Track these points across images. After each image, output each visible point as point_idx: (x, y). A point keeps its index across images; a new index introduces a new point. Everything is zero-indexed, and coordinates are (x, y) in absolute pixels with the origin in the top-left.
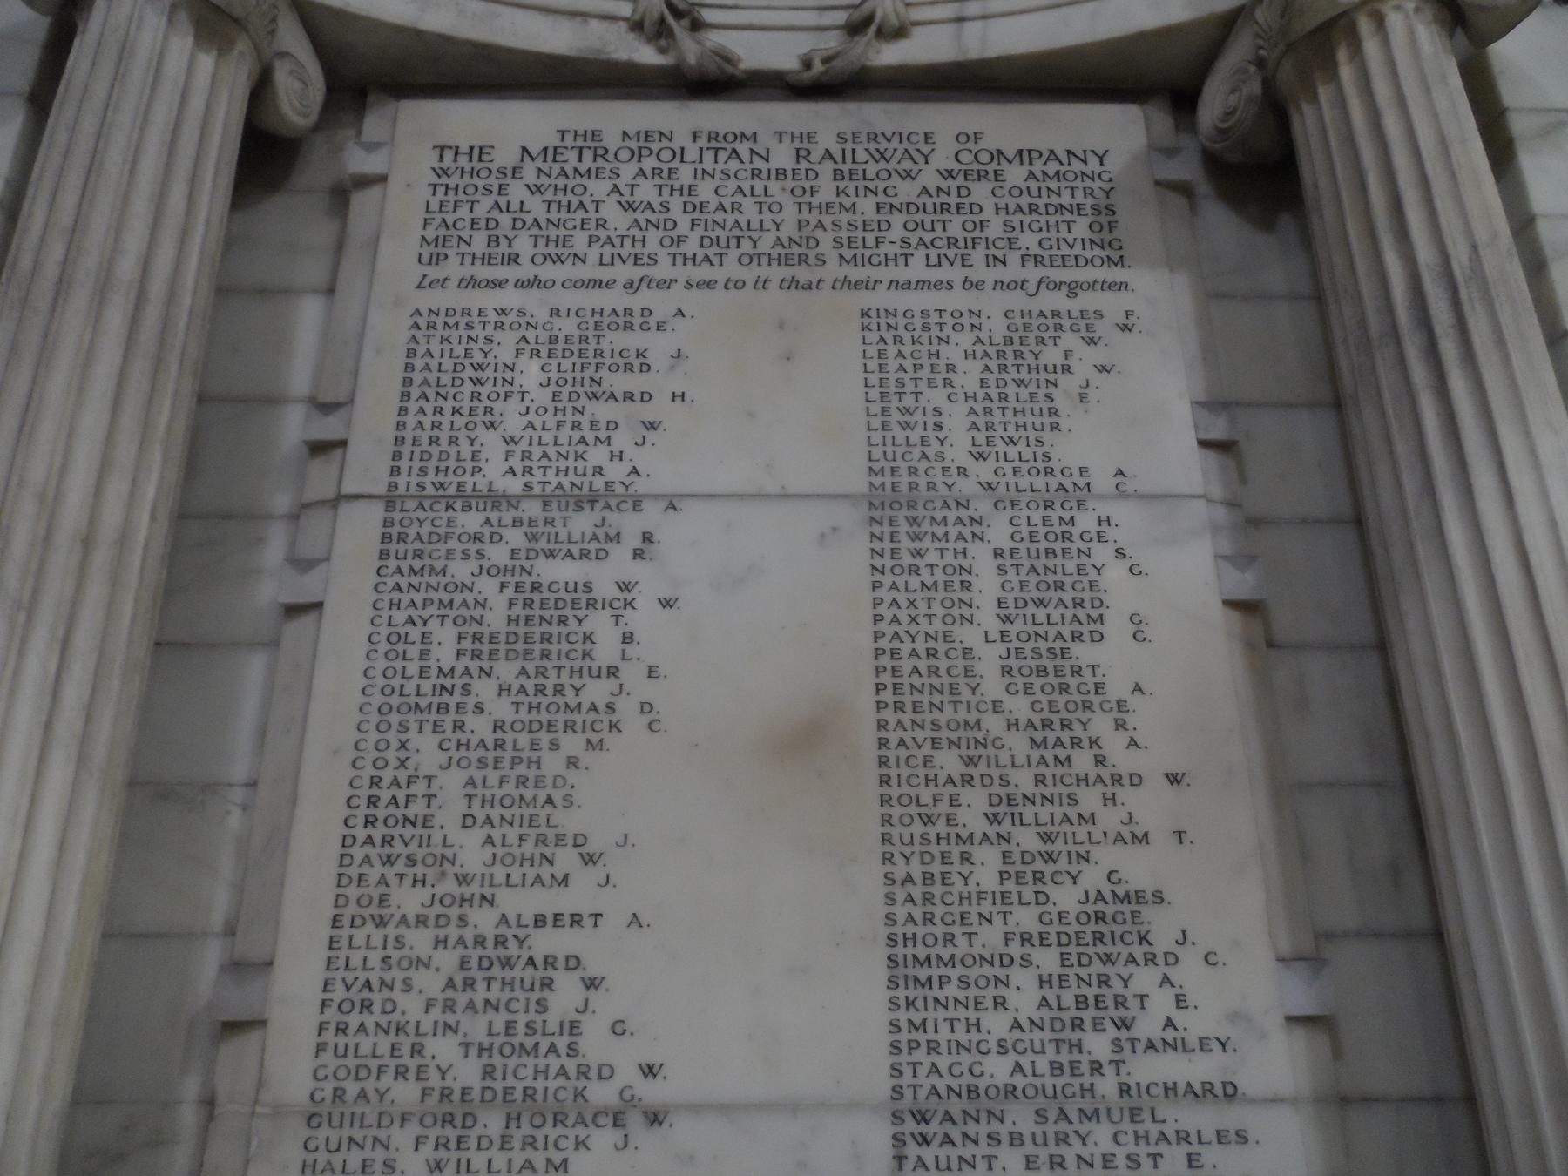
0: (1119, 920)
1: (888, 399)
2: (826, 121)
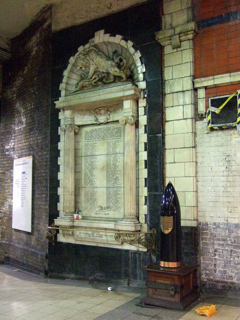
0: (117, 178)
1: (108, 148)
2: (105, 126)
